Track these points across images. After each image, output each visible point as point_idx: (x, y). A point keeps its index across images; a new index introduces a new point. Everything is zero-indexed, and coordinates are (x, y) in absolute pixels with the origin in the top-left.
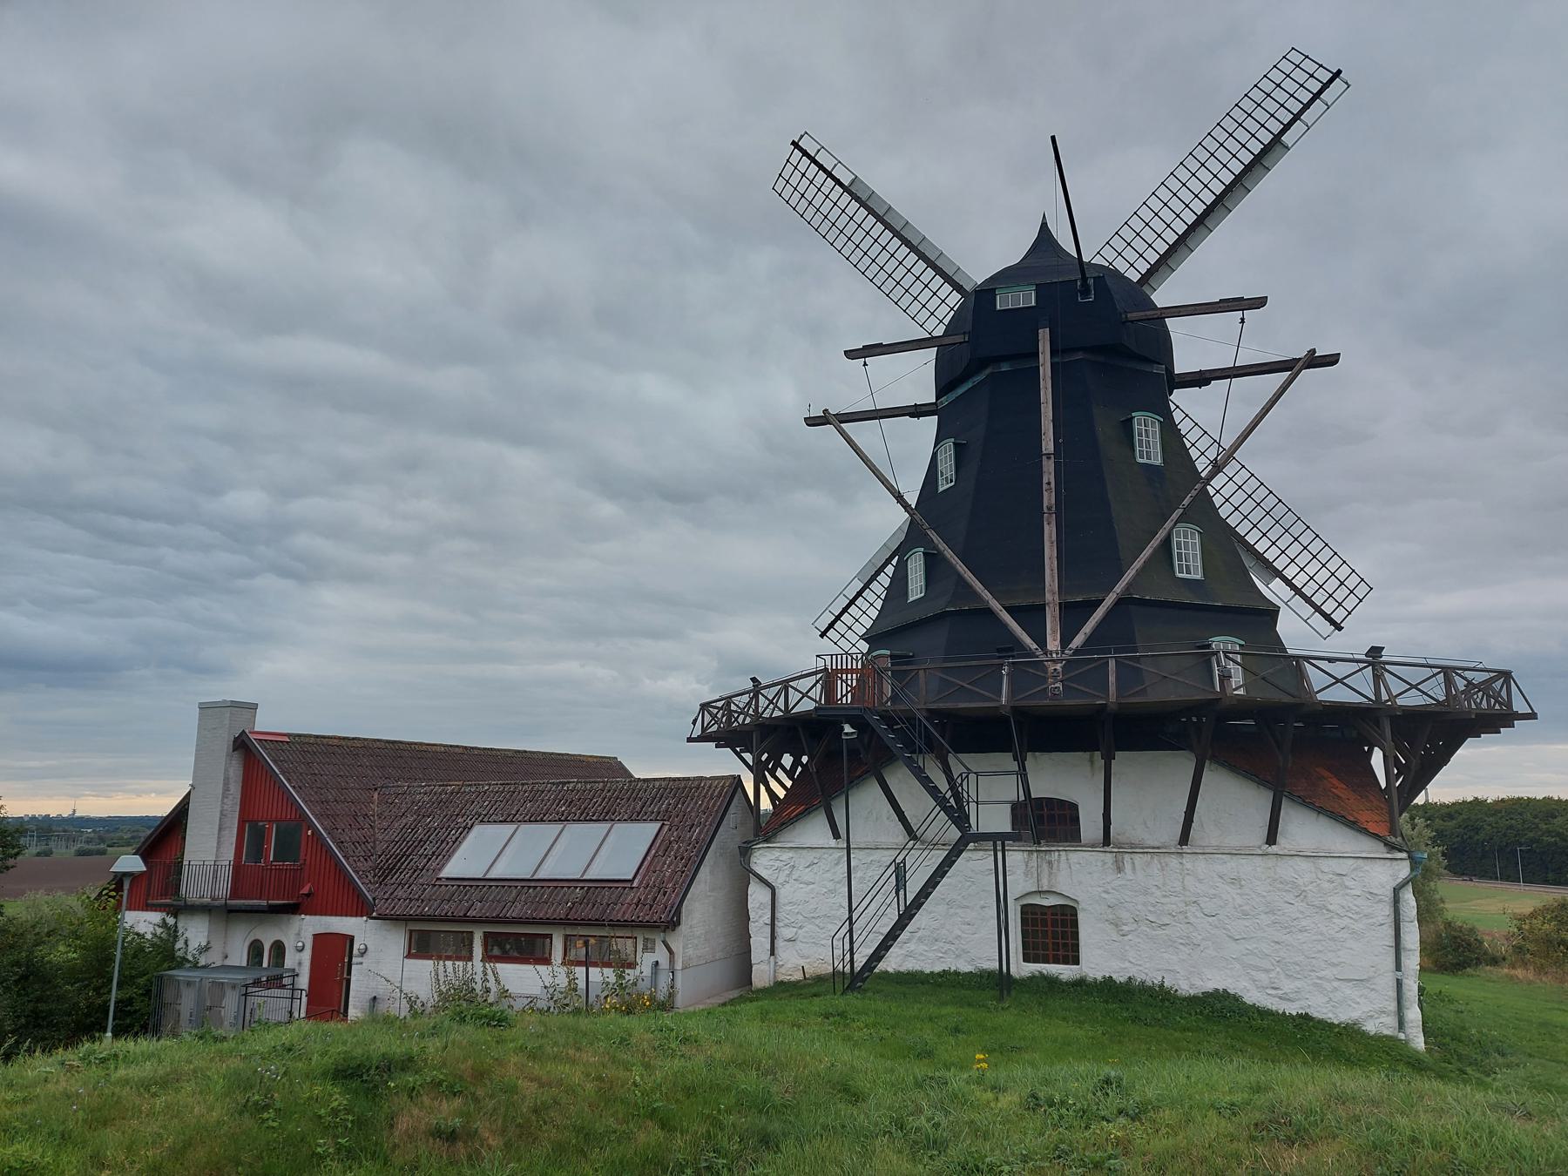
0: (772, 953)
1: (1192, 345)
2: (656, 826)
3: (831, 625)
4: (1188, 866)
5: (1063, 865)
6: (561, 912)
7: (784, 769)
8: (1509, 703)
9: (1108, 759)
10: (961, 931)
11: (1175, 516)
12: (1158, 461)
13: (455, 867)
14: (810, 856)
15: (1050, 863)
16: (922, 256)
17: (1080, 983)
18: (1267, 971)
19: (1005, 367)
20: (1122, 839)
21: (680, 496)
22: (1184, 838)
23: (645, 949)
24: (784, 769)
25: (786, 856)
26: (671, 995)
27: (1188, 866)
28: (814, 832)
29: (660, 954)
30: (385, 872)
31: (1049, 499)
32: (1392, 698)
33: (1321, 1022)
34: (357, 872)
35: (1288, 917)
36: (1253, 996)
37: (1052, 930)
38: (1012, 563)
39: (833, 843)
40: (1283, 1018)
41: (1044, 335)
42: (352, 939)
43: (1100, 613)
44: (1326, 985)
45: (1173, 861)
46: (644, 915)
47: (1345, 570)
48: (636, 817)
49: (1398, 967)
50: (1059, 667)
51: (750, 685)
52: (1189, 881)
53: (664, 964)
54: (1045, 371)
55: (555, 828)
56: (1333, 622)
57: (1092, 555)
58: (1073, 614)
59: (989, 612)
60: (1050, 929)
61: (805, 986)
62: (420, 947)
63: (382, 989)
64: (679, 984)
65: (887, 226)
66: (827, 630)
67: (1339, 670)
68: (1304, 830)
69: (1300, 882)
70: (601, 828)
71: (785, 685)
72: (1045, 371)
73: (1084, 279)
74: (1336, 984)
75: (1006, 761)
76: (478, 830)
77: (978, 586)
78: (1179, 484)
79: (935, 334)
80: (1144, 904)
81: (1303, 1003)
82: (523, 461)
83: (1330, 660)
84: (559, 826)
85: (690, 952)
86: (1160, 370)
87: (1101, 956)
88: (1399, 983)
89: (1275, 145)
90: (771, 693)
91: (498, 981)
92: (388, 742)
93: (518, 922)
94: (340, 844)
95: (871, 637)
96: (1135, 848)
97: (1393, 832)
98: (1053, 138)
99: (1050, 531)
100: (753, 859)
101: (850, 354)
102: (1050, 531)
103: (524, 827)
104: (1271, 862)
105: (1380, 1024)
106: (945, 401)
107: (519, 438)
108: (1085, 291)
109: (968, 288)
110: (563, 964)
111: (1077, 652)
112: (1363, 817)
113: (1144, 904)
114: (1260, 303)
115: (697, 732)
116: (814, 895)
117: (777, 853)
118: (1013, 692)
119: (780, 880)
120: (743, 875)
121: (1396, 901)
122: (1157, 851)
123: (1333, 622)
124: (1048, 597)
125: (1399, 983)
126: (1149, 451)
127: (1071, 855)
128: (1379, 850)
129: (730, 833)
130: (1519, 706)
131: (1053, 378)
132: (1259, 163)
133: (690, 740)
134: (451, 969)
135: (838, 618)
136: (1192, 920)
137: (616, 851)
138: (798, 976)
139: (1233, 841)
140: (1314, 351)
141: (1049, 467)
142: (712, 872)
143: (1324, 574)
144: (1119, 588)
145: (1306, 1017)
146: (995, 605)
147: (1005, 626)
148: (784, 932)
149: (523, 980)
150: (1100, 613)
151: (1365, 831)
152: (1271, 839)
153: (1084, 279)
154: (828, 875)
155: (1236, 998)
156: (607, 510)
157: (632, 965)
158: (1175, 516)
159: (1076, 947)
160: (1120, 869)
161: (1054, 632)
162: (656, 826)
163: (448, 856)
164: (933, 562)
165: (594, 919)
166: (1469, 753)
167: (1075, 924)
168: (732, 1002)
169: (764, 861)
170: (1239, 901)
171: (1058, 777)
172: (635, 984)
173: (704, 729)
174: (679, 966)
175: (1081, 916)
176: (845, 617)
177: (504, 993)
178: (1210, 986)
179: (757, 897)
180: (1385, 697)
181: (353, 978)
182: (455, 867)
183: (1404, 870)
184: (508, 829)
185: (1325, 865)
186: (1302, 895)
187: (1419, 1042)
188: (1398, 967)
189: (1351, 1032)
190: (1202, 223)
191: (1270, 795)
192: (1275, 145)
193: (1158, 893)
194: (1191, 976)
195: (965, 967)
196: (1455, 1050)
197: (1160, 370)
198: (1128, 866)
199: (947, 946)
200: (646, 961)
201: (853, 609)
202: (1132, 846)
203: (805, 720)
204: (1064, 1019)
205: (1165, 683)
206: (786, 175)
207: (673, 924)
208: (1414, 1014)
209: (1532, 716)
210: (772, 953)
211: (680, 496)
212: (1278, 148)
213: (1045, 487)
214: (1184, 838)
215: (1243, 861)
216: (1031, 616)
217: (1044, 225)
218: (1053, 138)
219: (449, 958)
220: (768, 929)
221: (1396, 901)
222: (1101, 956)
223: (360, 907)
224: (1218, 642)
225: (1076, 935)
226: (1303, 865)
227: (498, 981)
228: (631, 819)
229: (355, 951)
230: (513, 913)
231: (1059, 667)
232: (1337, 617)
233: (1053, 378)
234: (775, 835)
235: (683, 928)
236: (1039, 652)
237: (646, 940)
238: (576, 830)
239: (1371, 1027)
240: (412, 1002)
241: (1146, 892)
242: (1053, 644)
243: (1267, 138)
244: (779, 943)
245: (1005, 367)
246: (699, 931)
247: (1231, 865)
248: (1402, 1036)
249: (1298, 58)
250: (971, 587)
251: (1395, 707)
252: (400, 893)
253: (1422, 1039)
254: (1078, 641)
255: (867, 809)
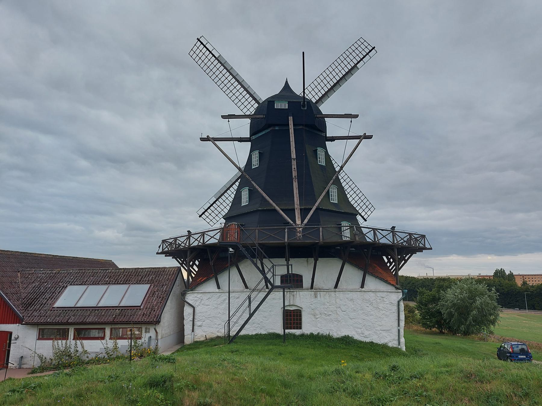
0: (193, 331)
1: (333, 128)
2: (148, 286)
3: (203, 213)
4: (337, 295)
5: (298, 296)
6: (111, 319)
7: (196, 265)
8: (425, 245)
9: (288, 261)
10: (269, 321)
11: (331, 182)
12: (324, 164)
13: (60, 303)
14: (209, 296)
15: (293, 295)
16: (242, 86)
17: (302, 335)
18: (361, 329)
19: (277, 128)
20: (317, 287)
21: (116, 161)
22: (336, 287)
23: (146, 332)
24: (196, 265)
25: (199, 296)
26: (156, 349)
27: (337, 295)
28: (210, 287)
29: (152, 333)
30: (27, 305)
31: (294, 174)
32: (398, 242)
33: (376, 344)
34: (15, 306)
35: (360, 311)
36: (357, 337)
37: (292, 318)
38: (283, 194)
39: (217, 290)
40: (366, 343)
41: (291, 118)
42: (11, 333)
43: (312, 212)
44: (378, 332)
45: (333, 294)
46: (145, 319)
47: (368, 203)
48: (139, 282)
49: (399, 326)
50: (301, 229)
51: (187, 233)
52: (338, 300)
53: (153, 337)
54: (292, 131)
55: (105, 287)
56: (364, 219)
57: (308, 195)
58: (304, 212)
59: (275, 210)
60: (292, 318)
61: (207, 342)
62: (42, 336)
63: (25, 352)
64: (159, 344)
65: (231, 74)
66: (202, 215)
67: (384, 233)
68: (372, 283)
69: (371, 300)
70: (125, 287)
71: (203, 234)
72: (292, 131)
73: (304, 101)
74: (381, 332)
75: (283, 261)
76: (70, 288)
77: (271, 202)
78: (330, 173)
79: (246, 114)
80: (324, 308)
81: (371, 338)
82: (46, 140)
83: (382, 230)
84: (106, 286)
85: (163, 332)
86: (323, 134)
87: (309, 327)
88: (399, 330)
89: (355, 67)
90: (196, 236)
91: (83, 347)
92: (22, 253)
93: (87, 323)
94: (6, 294)
95: (228, 218)
96: (320, 290)
97: (397, 284)
98: (303, 53)
99: (295, 185)
100: (186, 297)
101: (224, 117)
102: (295, 185)
103: (91, 287)
104: (363, 293)
105: (393, 344)
106: (254, 137)
107: (46, 130)
108: (304, 106)
109: (317, 105)
110: (111, 339)
111: (306, 225)
112: (389, 279)
113: (324, 308)
114: (356, 116)
115: (161, 250)
116: (212, 310)
117: (196, 295)
118: (288, 239)
119: (197, 303)
120: (182, 303)
121: (399, 305)
122: (327, 291)
123: (364, 219)
124: (296, 206)
125: (399, 330)
126: (322, 161)
127: (300, 292)
128: (393, 289)
129: (177, 289)
130: (427, 246)
131: (288, 134)
132: (350, 72)
133: (158, 253)
134: (61, 344)
135: (206, 211)
136: (338, 313)
137: (135, 295)
138: (202, 339)
139: (351, 287)
140: (365, 134)
141: (294, 163)
142: (171, 303)
143: (362, 203)
144: (317, 204)
145: (372, 342)
146: (277, 208)
147: (281, 216)
148: (197, 323)
149: (93, 347)
150: (312, 212)
151: (390, 284)
152: (362, 286)
153: (304, 101)
154: (215, 302)
155: (352, 338)
156: (84, 163)
157: (140, 338)
158: (331, 182)
159: (301, 324)
160: (316, 297)
161: (299, 218)
162: (148, 286)
163: (57, 299)
164: (252, 193)
165: (120, 320)
166: (415, 259)
167: (301, 316)
168: (178, 351)
169: (190, 298)
170: (353, 306)
171: (301, 267)
172: (142, 345)
173: (163, 250)
174: (159, 337)
175: (303, 314)
176: (209, 210)
177: (86, 352)
178: (343, 334)
179: (188, 311)
180: (396, 242)
181: (11, 349)
182: (60, 303)
183: (400, 295)
184: (84, 287)
185: (379, 294)
186: (371, 304)
187: (404, 349)
188: (399, 326)
189: (384, 347)
190: (332, 89)
191: (363, 273)
192: (355, 67)
193: (328, 304)
194: (338, 332)
195: (263, 332)
196: (413, 351)
197: (323, 134)
198: (319, 296)
199: (258, 325)
200: (145, 337)
201: (212, 208)
202: (320, 289)
203: (212, 247)
204: (308, 347)
205: (324, 236)
206: (194, 50)
207: (158, 322)
208: (403, 340)
209: (431, 249)
210: (193, 331)
211: (116, 161)
212: (356, 68)
213: (293, 170)
214: (336, 287)
215: (354, 293)
216: (291, 212)
217: (287, 82)
218: (303, 53)
219: (60, 339)
220: (192, 323)
221: (399, 305)
222: (309, 327)
223: (17, 320)
224: (344, 223)
225: (301, 320)
226: (372, 294)
227: (83, 347)
228: (137, 283)
229: (13, 338)
230: (89, 320)
231: (301, 229)
232: (365, 217)
233: (288, 134)
234: (195, 288)
235: (161, 323)
236: (294, 225)
237: (146, 328)
238: (113, 287)
239: (390, 345)
240: (41, 357)
241: (324, 304)
242: (298, 222)
243: (353, 65)
244: (195, 327)
245: (277, 128)
246: (166, 324)
247: (350, 295)
248: (400, 347)
249: (362, 41)
250: (268, 202)
251: (379, 243)
252: (35, 314)
253: (405, 348)
254: (306, 221)
255: (231, 279)
